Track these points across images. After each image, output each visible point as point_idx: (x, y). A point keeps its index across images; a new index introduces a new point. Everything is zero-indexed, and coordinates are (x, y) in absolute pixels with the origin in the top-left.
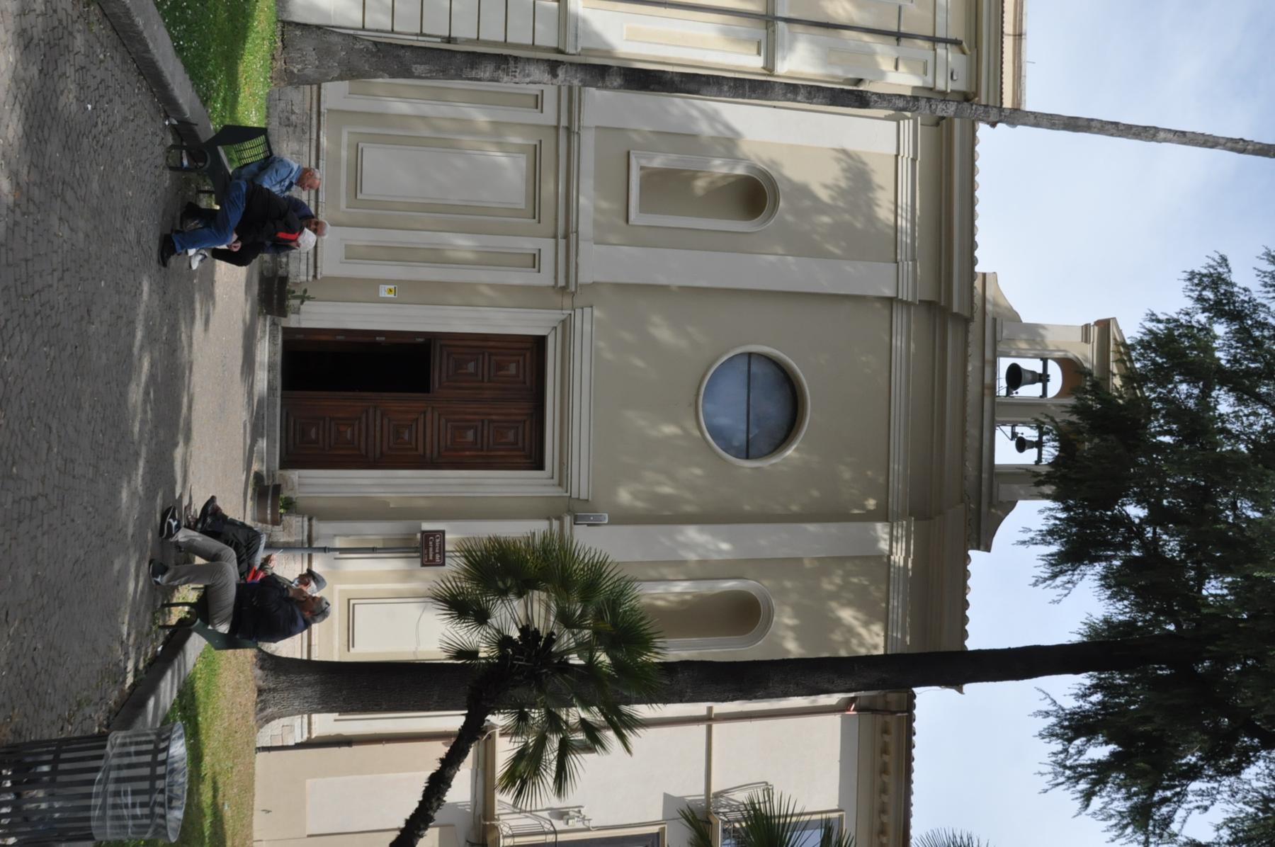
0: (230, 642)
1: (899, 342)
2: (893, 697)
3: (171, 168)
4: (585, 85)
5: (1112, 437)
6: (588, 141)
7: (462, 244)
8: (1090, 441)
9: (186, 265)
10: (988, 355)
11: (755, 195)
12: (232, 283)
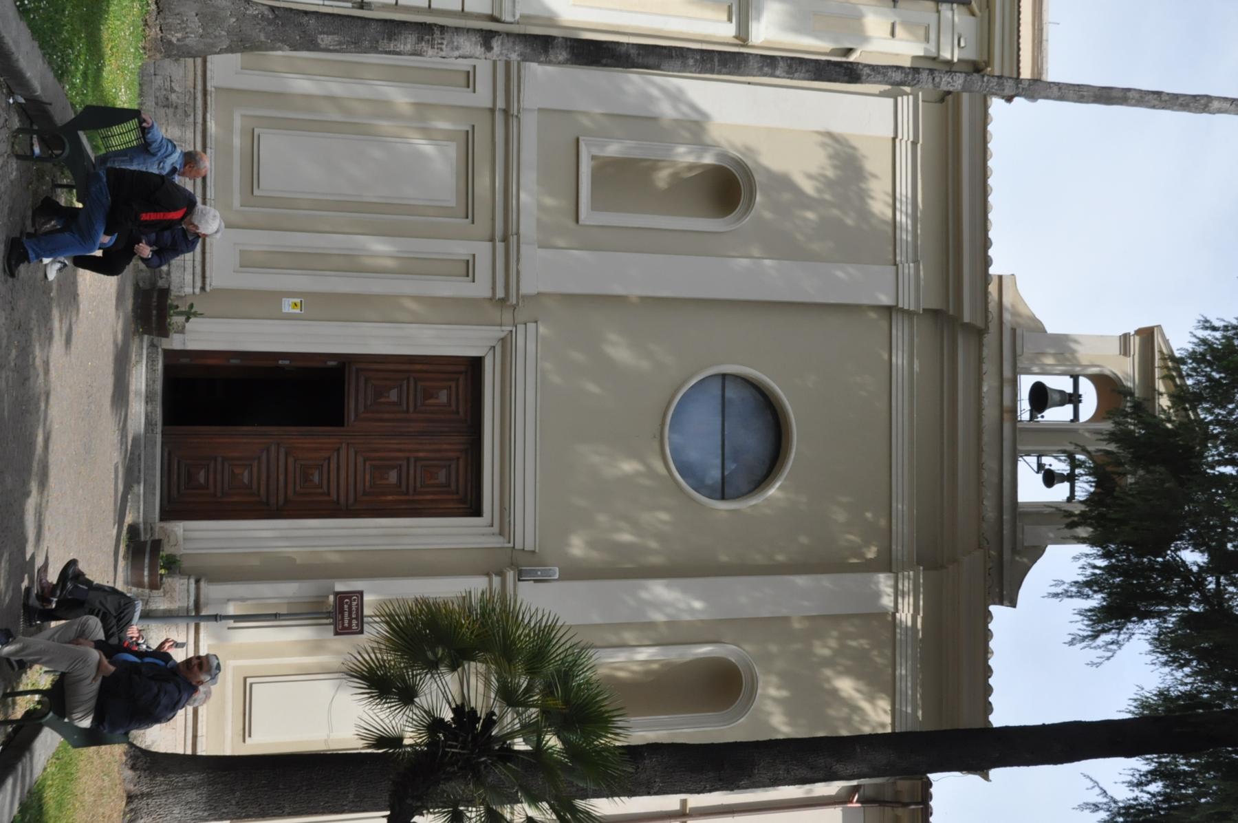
0: (92, 738)
1: (899, 360)
2: (904, 785)
3: (18, 157)
4: (525, 60)
5: (1160, 469)
6: (529, 129)
7: (380, 247)
8: (1134, 473)
9: (40, 275)
10: (1007, 373)
11: (727, 187)
12: (99, 294)
